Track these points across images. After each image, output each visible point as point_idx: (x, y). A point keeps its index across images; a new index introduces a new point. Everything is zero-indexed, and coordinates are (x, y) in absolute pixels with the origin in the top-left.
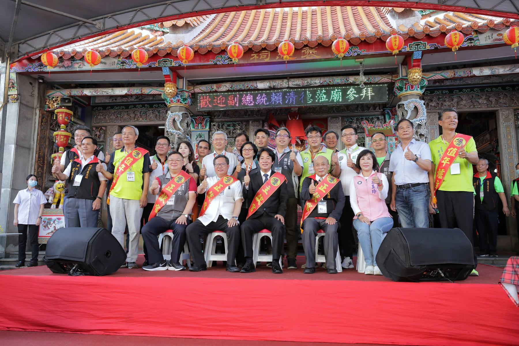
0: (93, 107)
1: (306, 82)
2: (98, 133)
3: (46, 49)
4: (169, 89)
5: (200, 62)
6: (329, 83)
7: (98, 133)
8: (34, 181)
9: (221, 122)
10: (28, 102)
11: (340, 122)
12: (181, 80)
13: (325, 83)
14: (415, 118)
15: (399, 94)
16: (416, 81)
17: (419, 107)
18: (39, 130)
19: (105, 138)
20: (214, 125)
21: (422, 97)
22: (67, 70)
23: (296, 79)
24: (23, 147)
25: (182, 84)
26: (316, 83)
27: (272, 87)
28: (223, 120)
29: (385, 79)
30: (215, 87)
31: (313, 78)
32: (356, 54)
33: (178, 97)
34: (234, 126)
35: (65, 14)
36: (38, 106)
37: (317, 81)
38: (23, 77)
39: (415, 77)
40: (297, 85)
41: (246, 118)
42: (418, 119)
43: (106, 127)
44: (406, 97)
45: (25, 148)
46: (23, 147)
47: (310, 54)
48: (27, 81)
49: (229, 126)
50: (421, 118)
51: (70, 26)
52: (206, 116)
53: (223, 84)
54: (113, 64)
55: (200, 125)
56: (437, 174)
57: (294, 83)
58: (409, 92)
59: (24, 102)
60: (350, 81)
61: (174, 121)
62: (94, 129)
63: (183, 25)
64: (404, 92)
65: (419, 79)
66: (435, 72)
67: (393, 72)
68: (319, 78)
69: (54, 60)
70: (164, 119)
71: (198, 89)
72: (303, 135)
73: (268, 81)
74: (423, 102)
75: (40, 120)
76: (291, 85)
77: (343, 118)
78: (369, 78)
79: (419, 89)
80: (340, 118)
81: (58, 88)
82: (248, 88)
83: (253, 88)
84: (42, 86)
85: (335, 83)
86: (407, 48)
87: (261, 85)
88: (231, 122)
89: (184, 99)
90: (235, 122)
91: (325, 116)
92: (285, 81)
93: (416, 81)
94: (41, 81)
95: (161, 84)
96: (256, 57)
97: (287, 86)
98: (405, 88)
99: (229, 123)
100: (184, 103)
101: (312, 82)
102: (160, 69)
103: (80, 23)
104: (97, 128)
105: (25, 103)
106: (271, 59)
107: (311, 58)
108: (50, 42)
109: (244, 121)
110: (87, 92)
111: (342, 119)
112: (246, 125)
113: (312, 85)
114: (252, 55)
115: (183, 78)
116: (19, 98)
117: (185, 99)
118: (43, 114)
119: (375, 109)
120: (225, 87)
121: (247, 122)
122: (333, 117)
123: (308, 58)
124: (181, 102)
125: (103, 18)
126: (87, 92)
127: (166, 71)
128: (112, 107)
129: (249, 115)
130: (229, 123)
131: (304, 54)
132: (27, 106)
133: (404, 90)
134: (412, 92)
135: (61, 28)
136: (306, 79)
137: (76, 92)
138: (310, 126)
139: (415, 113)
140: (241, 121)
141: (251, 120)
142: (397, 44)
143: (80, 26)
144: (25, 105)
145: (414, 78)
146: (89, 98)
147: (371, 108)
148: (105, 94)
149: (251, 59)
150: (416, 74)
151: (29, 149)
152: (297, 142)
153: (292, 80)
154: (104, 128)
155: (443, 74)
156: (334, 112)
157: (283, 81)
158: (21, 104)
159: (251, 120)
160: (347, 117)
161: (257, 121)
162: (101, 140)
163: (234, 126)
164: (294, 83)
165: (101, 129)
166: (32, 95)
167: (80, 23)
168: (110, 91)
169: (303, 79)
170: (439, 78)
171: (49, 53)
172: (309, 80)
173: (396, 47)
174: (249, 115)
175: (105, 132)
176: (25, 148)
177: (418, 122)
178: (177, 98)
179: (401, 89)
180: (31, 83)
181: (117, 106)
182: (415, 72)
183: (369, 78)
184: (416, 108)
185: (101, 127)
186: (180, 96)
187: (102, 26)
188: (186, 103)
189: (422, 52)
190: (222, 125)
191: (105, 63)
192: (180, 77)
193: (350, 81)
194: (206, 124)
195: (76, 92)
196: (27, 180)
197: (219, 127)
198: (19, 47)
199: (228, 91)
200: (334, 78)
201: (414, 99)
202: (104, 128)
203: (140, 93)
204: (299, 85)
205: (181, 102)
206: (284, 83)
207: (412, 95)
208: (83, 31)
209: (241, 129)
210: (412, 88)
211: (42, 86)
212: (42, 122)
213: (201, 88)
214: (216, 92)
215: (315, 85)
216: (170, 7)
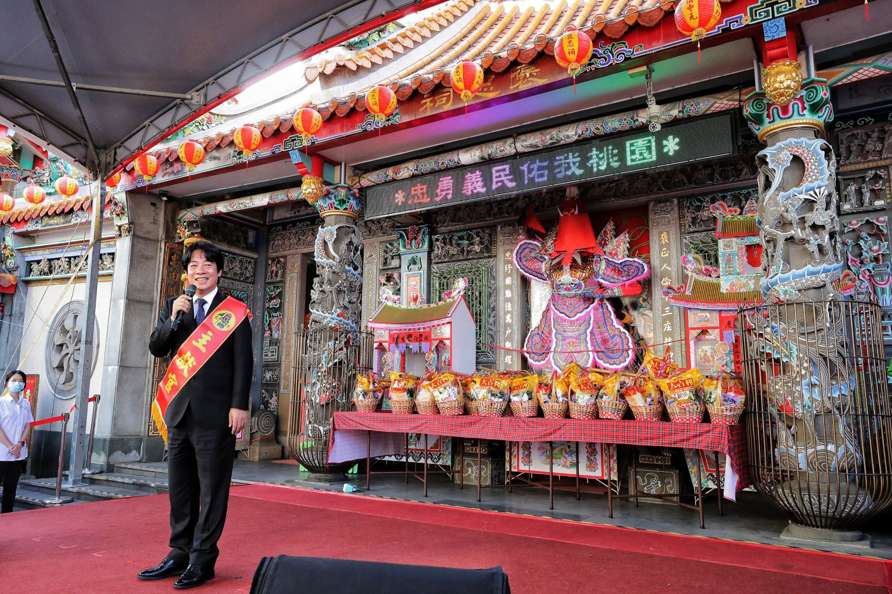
0: (271, 227)
1: (548, 137)
2: (274, 269)
3: (141, 151)
4: (308, 188)
5: (342, 131)
6: (597, 132)
7: (274, 269)
8: (17, 383)
9: (450, 232)
10: (148, 232)
11: (676, 209)
12: (337, 168)
13: (587, 134)
14: (798, 185)
15: (759, 131)
16: (782, 95)
17: (805, 156)
18: (166, 272)
19: (284, 274)
20: (437, 240)
21: (828, 132)
22: (446, 160)
23: (528, 135)
24: (139, 302)
25: (338, 175)
26: (568, 137)
27: (486, 157)
28: (453, 228)
29: (722, 103)
30: (390, 172)
31: (562, 128)
32: (621, 59)
33: (330, 199)
34: (470, 238)
35: (142, 92)
36: (164, 237)
37: (571, 133)
38: (138, 196)
39: (777, 85)
40: (531, 146)
41: (490, 221)
42: (803, 187)
43: (285, 257)
44: (774, 136)
45: (144, 302)
46: (139, 302)
47: (529, 78)
48: (146, 202)
49: (461, 238)
50: (811, 185)
51: (165, 109)
52: (422, 224)
53: (404, 165)
54: (226, 158)
55: (413, 242)
56: (162, 567)
57: (525, 143)
58: (779, 123)
59: (139, 233)
60: (640, 120)
61: (325, 243)
62: (270, 262)
63: (335, 70)
64: (767, 126)
65: (788, 87)
66: (860, 62)
67: (746, 81)
68: (575, 125)
69: (149, 165)
70: (312, 244)
71: (368, 180)
72: (593, 244)
73: (478, 147)
74: (821, 142)
75: (167, 258)
76: (521, 149)
77: (680, 199)
78: (684, 107)
79: (806, 112)
80: (676, 202)
81: (197, 205)
82: (444, 166)
83: (452, 164)
84: (170, 206)
85: (608, 131)
86: (744, 18)
87: (466, 157)
88: (464, 230)
89: (340, 201)
90: (471, 230)
91: (642, 199)
92: (510, 141)
93: (782, 95)
94: (165, 199)
95: (297, 183)
96: (429, 104)
97: (513, 151)
98: (768, 116)
99: (460, 234)
100: (341, 209)
101: (561, 136)
102: (285, 155)
103: (178, 101)
104: (273, 260)
105: (143, 235)
106: (454, 103)
107: (529, 86)
108: (148, 137)
109: (487, 227)
110: (222, 207)
111: (679, 202)
112: (490, 235)
113: (562, 142)
114: (423, 102)
115: (340, 164)
116: (133, 229)
117: (342, 202)
118: (171, 249)
119: (711, 177)
120: (406, 171)
121: (493, 228)
122: (659, 201)
123: (523, 87)
124: (336, 208)
125: (203, 87)
126: (222, 207)
127: (296, 157)
128: (294, 224)
129: (495, 215)
130: (460, 234)
131: (515, 81)
132: (146, 239)
133: (767, 120)
134: (788, 122)
135: (157, 115)
136: (548, 131)
137: (209, 209)
138: (610, 227)
139: (798, 173)
140: (481, 228)
141: (499, 223)
142: (696, 14)
143: (177, 106)
144: (142, 238)
145: (776, 89)
146: (219, 216)
147: (745, 170)
148: (242, 207)
149: (421, 110)
150: (782, 78)
151: (151, 303)
152: (574, 261)
153: (523, 137)
154: (282, 260)
155: (880, 63)
156: (660, 189)
157: (505, 143)
158: (134, 236)
159: (499, 223)
160: (689, 197)
161: (509, 225)
162: (279, 279)
163: (470, 238)
164: (525, 143)
165: (279, 262)
166: (155, 222)
167: (178, 101)
168: (248, 202)
169: (544, 132)
170: (871, 75)
171: (145, 157)
172: (554, 132)
173: (694, 23)
174: (495, 215)
175: (284, 268)
176: (144, 302)
177: (803, 196)
178: (328, 201)
179: (759, 120)
180: (153, 204)
181: (301, 221)
182: (779, 73)
183: (684, 107)
184: (797, 160)
185: (278, 257)
186: (333, 197)
187: (202, 98)
188: (346, 209)
189: (786, 20)
190: (451, 239)
191: (219, 158)
192: (335, 163)
193: (640, 120)
194: (423, 240)
195: (209, 209)
196: (7, 380)
197: (445, 243)
198: (115, 153)
199: (414, 176)
200: (606, 118)
201: (793, 140)
202: (282, 260)
203: (286, 199)
204: (536, 146)
205: (336, 208)
206: (507, 148)
207: (789, 130)
208: (183, 112)
209: (481, 243)
210: (785, 110)
211: (170, 206)
212: (170, 260)
213: (369, 178)
214: (394, 180)
215: (569, 141)
216: (289, 44)
